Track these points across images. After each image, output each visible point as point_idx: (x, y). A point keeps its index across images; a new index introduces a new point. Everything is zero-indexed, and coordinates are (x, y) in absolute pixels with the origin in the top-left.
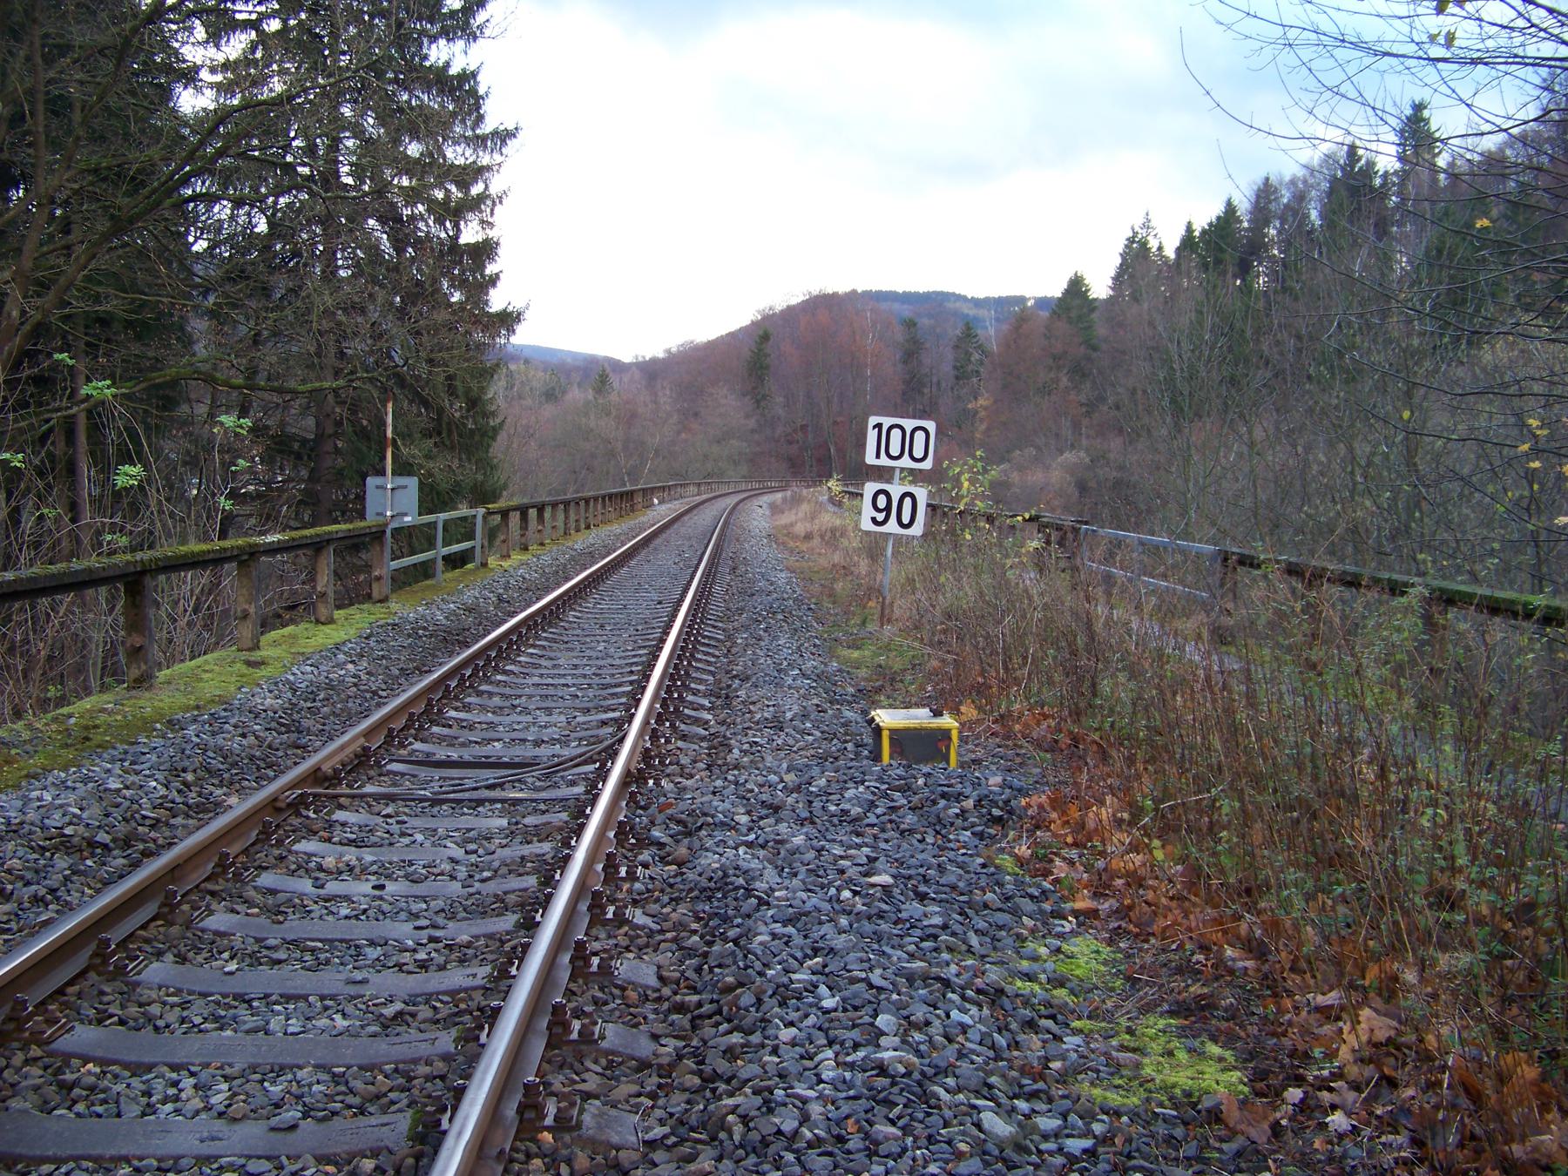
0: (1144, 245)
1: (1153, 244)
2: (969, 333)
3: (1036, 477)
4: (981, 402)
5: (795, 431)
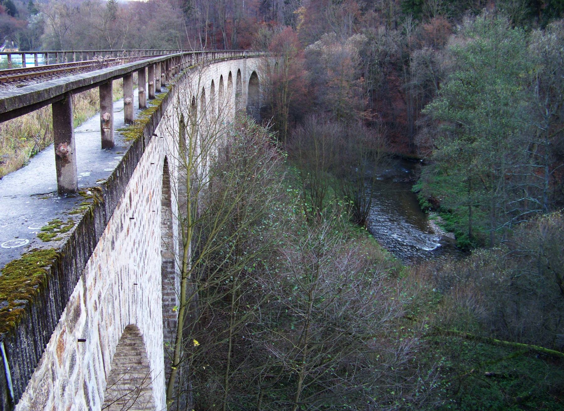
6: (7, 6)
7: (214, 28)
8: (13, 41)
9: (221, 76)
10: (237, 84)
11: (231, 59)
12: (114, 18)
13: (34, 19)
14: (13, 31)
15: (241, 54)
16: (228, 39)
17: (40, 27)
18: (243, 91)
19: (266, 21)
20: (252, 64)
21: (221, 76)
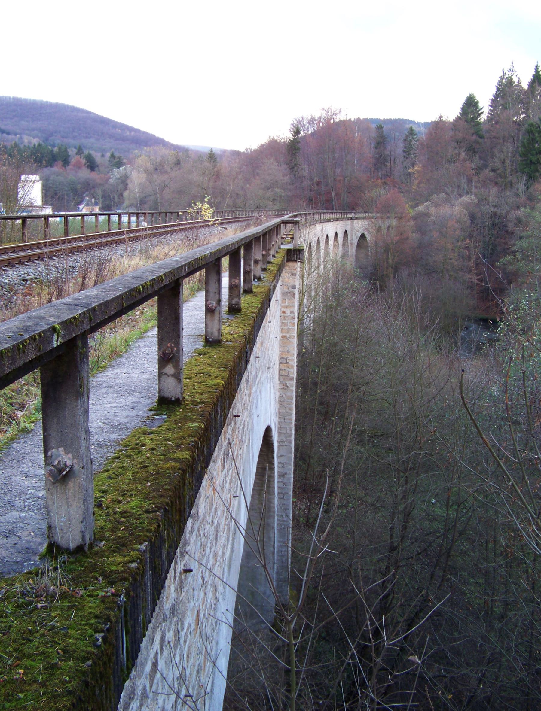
0: (510, 80)
1: (515, 79)
2: (411, 132)
3: (445, 210)
4: (416, 168)
5: (313, 184)
6: (86, 160)
7: (323, 187)
8: (94, 197)
9: (327, 236)
10: (344, 245)
11: (337, 220)
12: (217, 175)
13: (117, 173)
14: (93, 187)
15: (348, 216)
16: (338, 200)
17: (124, 181)
18: (349, 253)
19: (381, 178)
20: (358, 226)
21: (327, 236)
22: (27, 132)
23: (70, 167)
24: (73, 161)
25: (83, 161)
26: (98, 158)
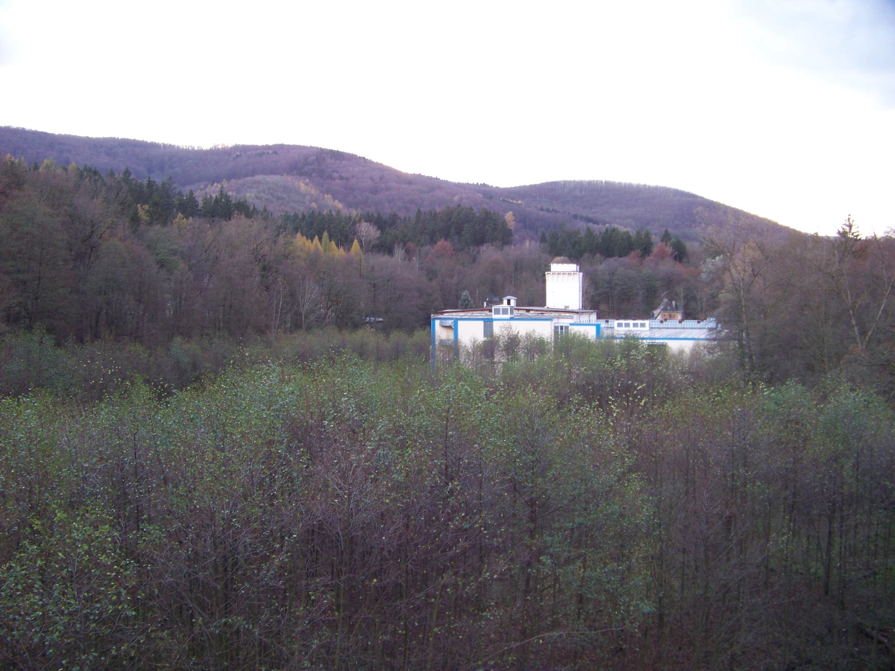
22: (618, 220)
23: (651, 257)
24: (655, 250)
25: (669, 250)
26: (691, 246)
